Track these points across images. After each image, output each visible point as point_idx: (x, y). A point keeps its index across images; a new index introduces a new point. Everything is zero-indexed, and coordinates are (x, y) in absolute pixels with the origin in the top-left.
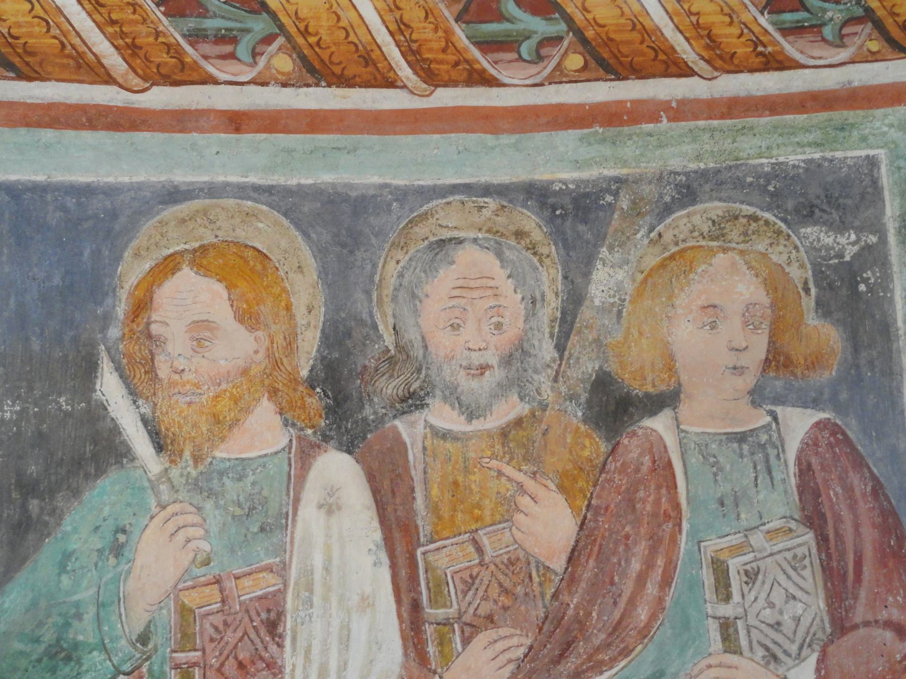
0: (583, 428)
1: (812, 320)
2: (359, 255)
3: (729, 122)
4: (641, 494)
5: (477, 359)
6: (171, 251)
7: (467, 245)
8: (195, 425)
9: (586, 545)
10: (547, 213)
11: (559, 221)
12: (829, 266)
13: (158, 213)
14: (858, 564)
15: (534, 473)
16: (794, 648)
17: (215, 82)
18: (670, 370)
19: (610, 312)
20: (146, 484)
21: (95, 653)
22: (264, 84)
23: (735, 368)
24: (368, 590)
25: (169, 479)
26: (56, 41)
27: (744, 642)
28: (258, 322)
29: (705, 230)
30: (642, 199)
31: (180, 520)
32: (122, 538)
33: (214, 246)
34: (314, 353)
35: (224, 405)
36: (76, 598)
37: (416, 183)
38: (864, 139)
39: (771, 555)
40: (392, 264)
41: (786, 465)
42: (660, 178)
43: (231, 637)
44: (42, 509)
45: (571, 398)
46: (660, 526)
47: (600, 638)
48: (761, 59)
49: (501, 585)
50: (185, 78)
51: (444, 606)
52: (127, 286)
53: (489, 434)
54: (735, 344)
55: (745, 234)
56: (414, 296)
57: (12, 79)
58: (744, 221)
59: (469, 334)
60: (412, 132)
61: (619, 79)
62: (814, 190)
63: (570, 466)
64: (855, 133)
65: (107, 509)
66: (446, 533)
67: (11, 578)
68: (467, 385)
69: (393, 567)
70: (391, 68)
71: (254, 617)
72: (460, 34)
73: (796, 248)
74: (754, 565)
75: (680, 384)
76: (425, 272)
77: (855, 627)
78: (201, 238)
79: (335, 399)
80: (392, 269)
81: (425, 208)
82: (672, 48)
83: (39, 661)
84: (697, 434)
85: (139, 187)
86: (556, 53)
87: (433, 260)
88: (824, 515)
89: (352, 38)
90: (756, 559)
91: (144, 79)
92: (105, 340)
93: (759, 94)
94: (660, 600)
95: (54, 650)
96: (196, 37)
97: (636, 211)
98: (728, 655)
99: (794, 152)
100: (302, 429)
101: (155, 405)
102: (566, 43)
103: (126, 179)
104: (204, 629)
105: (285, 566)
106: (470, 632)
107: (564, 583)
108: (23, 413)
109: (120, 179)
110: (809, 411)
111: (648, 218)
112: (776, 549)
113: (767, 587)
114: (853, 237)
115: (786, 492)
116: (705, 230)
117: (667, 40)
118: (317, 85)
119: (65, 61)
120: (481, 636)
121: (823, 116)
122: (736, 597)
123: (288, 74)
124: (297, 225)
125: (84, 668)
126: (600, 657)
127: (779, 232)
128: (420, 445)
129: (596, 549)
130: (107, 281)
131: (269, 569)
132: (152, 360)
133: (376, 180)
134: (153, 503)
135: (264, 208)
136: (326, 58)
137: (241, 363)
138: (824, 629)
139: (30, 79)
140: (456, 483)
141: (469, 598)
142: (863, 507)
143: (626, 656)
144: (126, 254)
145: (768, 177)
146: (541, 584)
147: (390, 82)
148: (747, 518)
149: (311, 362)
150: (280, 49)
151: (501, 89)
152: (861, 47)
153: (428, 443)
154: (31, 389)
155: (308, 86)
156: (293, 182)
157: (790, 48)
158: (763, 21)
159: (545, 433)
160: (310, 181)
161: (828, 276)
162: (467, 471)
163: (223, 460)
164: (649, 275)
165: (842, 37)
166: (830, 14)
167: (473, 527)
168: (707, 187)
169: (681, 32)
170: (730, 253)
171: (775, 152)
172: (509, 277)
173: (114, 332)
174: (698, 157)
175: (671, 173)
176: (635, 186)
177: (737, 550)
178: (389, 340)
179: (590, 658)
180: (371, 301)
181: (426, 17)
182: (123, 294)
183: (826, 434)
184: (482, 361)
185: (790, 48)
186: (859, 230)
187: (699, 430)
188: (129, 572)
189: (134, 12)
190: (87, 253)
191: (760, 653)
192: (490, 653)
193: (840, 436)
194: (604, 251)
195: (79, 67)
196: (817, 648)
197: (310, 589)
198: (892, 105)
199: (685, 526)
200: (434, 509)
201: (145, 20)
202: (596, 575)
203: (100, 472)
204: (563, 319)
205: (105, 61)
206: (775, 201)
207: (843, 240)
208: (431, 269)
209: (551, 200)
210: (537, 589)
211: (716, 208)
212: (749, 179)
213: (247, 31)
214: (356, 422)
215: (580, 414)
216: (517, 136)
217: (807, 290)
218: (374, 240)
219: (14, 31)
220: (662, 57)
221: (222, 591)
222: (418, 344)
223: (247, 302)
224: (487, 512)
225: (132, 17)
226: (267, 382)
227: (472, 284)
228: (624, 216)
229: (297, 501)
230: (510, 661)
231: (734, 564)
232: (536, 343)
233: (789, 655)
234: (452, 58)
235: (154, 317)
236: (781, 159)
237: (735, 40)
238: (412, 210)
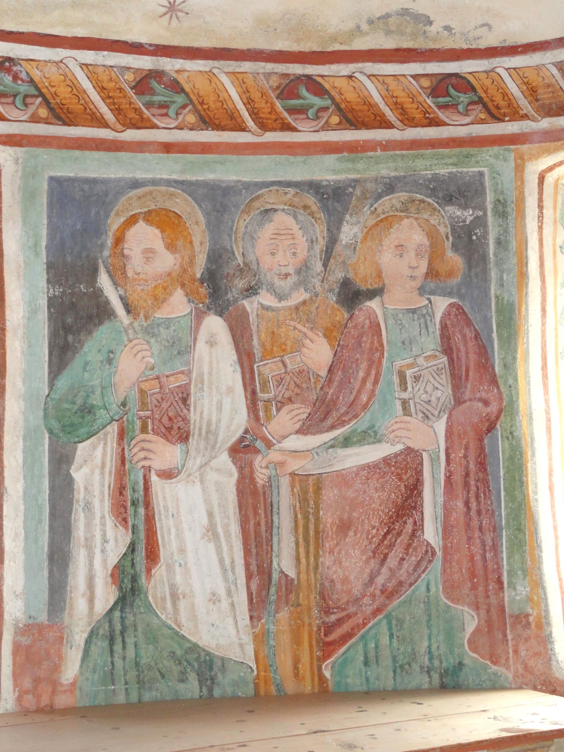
0: (336, 306)
1: (450, 253)
2: (226, 216)
3: (411, 152)
4: (365, 339)
5: (284, 270)
6: (134, 213)
7: (279, 212)
8: (145, 301)
9: (337, 364)
10: (319, 197)
11: (325, 201)
12: (459, 226)
13: (128, 193)
14: (467, 370)
15: (312, 328)
16: (436, 413)
17: (158, 127)
18: (380, 277)
19: (350, 247)
20: (122, 329)
21: (102, 410)
22: (181, 129)
23: (411, 277)
24: (230, 384)
25: (133, 328)
26: (82, 107)
27: (413, 410)
28: (176, 250)
29: (398, 207)
30: (367, 191)
31: (139, 347)
32: (112, 356)
33: (155, 210)
34: (203, 266)
35: (160, 290)
36: (91, 383)
37: (254, 180)
38: (477, 162)
39: (427, 368)
40: (241, 222)
41: (435, 325)
42: (376, 180)
43: (165, 405)
44: (74, 340)
45: (331, 290)
46: (373, 354)
47: (343, 409)
48: (427, 121)
49: (295, 383)
50: (143, 126)
51: (268, 393)
52: (112, 230)
53: (290, 308)
54: (412, 265)
55: (418, 209)
56: (253, 238)
57: (61, 125)
58: (417, 203)
59: (280, 257)
60: (254, 154)
61: (357, 129)
62: (452, 188)
63: (329, 325)
64: (473, 159)
65: (104, 341)
66: (268, 357)
67: (61, 373)
68: (279, 283)
69: (243, 373)
70: (244, 122)
71: (176, 396)
72: (278, 105)
73: (443, 217)
74: (419, 373)
75: (384, 285)
76: (258, 225)
77: (465, 402)
78: (149, 206)
79: (214, 289)
80: (242, 224)
81: (259, 193)
82: (384, 114)
83: (76, 413)
84: (392, 309)
85: (119, 180)
86: (325, 115)
87: (262, 220)
88: (452, 348)
89: (225, 106)
90: (419, 371)
91: (123, 125)
92: (101, 257)
93: (427, 138)
94: (373, 391)
95: (82, 408)
96: (149, 105)
97: (364, 196)
98: (405, 417)
99: (443, 168)
100: (197, 304)
101: (126, 290)
102: (330, 110)
103: (113, 176)
104: (152, 401)
105: (190, 372)
106: (281, 405)
107: (326, 383)
108: (63, 293)
109: (110, 176)
110: (446, 298)
111: (370, 201)
112: (429, 365)
113: (424, 383)
114: (471, 212)
115: (434, 337)
116: (398, 207)
117: (381, 110)
118: (207, 129)
119: (86, 116)
120: (285, 407)
121: (458, 150)
122: (410, 389)
123: (193, 124)
124: (196, 202)
125: (97, 417)
126: (343, 418)
127: (435, 209)
128: (255, 313)
129: (342, 366)
130: (103, 227)
131: (182, 372)
132: (125, 267)
133: (234, 178)
134: (125, 339)
135: (180, 191)
136: (212, 116)
137: (167, 270)
138: (451, 403)
139: (69, 125)
140: (273, 333)
141: (280, 389)
142: (471, 344)
143: (357, 417)
144: (112, 214)
145: (430, 181)
146: (315, 383)
147: (242, 128)
148: (415, 351)
149: (202, 270)
150: (189, 111)
151: (298, 133)
152: (476, 116)
153: (259, 312)
154: (67, 281)
155: (202, 130)
156: (194, 179)
157: (441, 115)
158: (429, 101)
159: (317, 308)
160: (202, 178)
161: (458, 232)
162: (279, 326)
163: (159, 318)
164: (370, 229)
165: (467, 111)
166: (462, 99)
167: (282, 354)
168: (399, 185)
169: (388, 106)
170: (410, 219)
171: (433, 168)
172: (300, 229)
173: (106, 253)
174: (396, 170)
175: (382, 177)
176: (363, 184)
177: (410, 366)
178: (240, 260)
179: (338, 419)
180: (231, 240)
181: (262, 96)
182: (110, 234)
183: (454, 309)
184: (286, 272)
185: (441, 115)
186: (474, 208)
187: (393, 307)
188: (115, 372)
189: (120, 92)
190: (93, 213)
191: (421, 415)
192: (289, 416)
193: (461, 311)
194: (347, 217)
195: (92, 119)
196: (447, 412)
197: (202, 383)
198: (491, 146)
199: (386, 354)
200: (263, 345)
201: (125, 97)
202: (342, 378)
203: (101, 323)
204: (327, 251)
205: (105, 117)
206: (433, 192)
207: (466, 214)
208: (261, 224)
209: (321, 191)
210: (313, 385)
211: (403, 196)
212: (421, 182)
213: (174, 102)
214: (224, 301)
215: (334, 299)
216: (305, 157)
217: (447, 238)
218: (233, 209)
219: (63, 102)
220: (378, 118)
221: (160, 383)
222: (254, 263)
223: (171, 239)
224: (289, 347)
225: (119, 95)
226: (180, 280)
227: (282, 232)
228: (358, 199)
229: (195, 339)
230: (300, 420)
231: (409, 373)
232: (313, 263)
233: (434, 416)
234: (273, 117)
235: (126, 246)
236: (437, 172)
237: (414, 111)
238: (252, 194)
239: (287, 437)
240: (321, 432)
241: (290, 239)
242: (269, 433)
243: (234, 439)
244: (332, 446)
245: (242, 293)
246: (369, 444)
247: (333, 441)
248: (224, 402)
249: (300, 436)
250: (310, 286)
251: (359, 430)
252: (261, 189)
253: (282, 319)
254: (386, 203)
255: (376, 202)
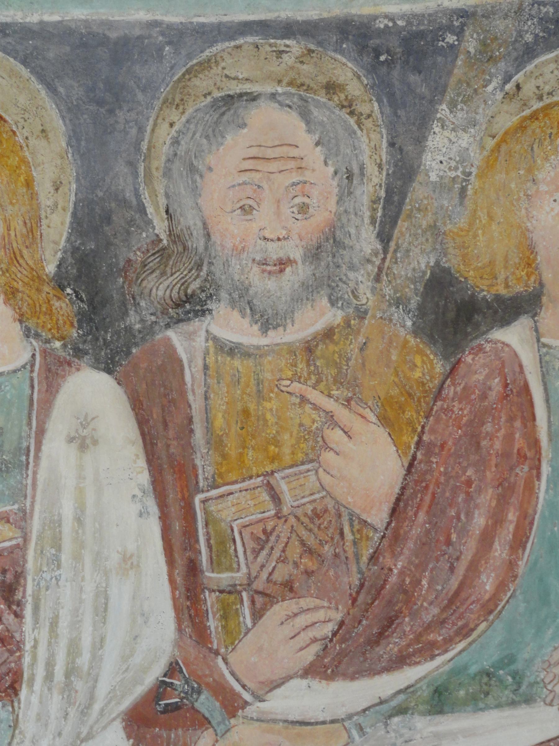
0: (412, 341)
2: (121, 115)
4: (488, 427)
7: (262, 103)
9: (415, 493)
10: (367, 60)
15: (349, 400)
18: (529, 265)
19: (450, 190)
24: (131, 547)
34: (63, 243)
37: (195, 20)
45: (398, 302)
46: (512, 469)
49: (303, 543)
51: (230, 569)
53: (291, 350)
56: (192, 169)
63: (395, 392)
66: (232, 477)
69: (164, 518)
75: (541, 285)
76: (207, 137)
79: (91, 303)
87: (217, 123)
94: (511, 565)
100: (48, 341)
107: (385, 542)
111: (502, 65)
120: (277, 608)
124: (42, 78)
126: (431, 637)
128: (200, 363)
129: (428, 498)
133: (143, 16)
140: (246, 412)
141: (261, 558)
146: (355, 543)
149: (59, 255)
153: (211, 360)
156: (34, 18)
160: (56, 18)
162: (260, 396)
164: (503, 140)
167: (268, 469)
172: (317, 144)
179: (418, 638)
184: (281, 254)
192: (287, 630)
194: (443, 110)
199: (545, 469)
202: (428, 532)
204: (388, 200)
214: (117, 333)
215: (409, 323)
218: (140, 96)
222: (198, 232)
224: (287, 450)
227: (270, 153)
228: (471, 62)
229: (41, 432)
230: (314, 640)
232: (353, 231)
238: (190, 57)
239: (278, 686)
240: (373, 672)
241: (290, 170)
242: (233, 674)
243: (140, 690)
244: (401, 711)
245: (164, 312)
246: (499, 706)
247: (402, 697)
248: (113, 592)
249: (317, 684)
250: (345, 290)
251: (473, 669)
252: (213, 42)
253: (268, 376)
254: (547, 70)
255: (519, 67)
